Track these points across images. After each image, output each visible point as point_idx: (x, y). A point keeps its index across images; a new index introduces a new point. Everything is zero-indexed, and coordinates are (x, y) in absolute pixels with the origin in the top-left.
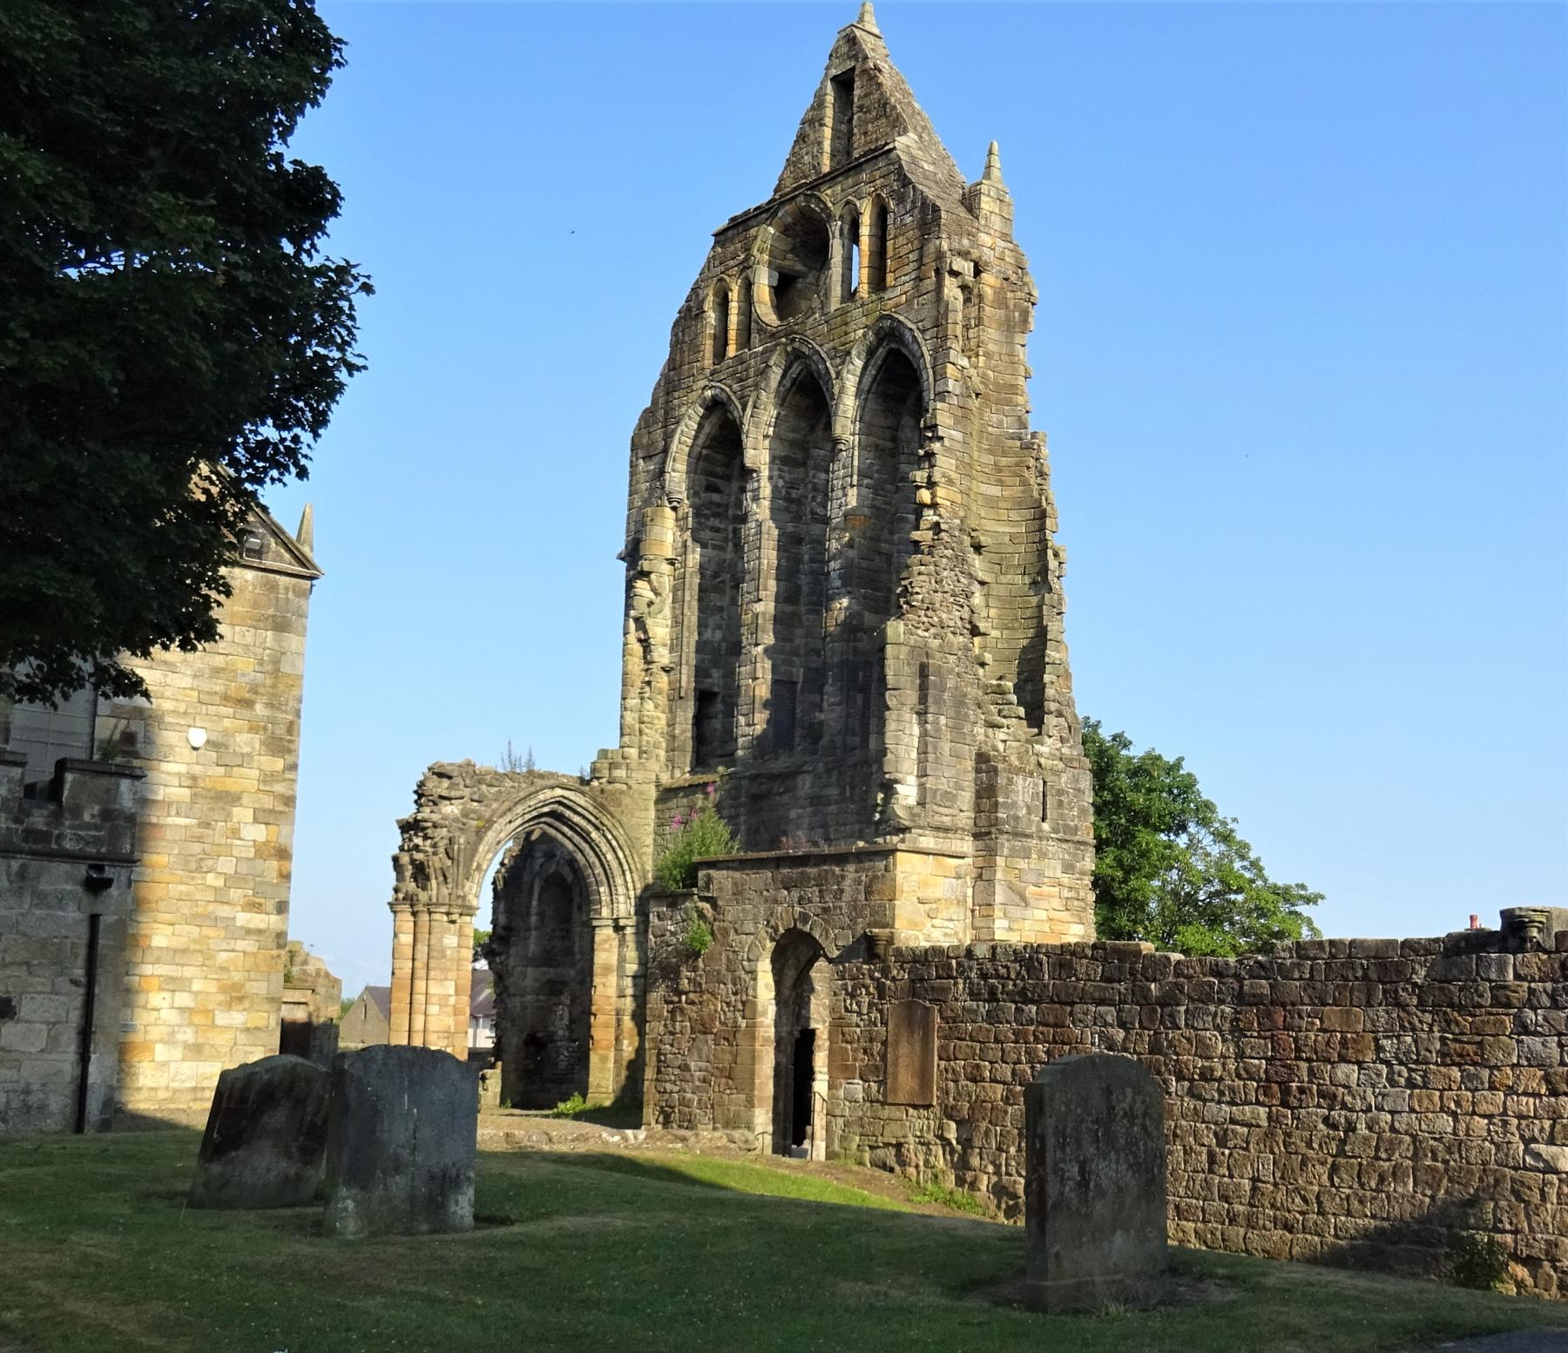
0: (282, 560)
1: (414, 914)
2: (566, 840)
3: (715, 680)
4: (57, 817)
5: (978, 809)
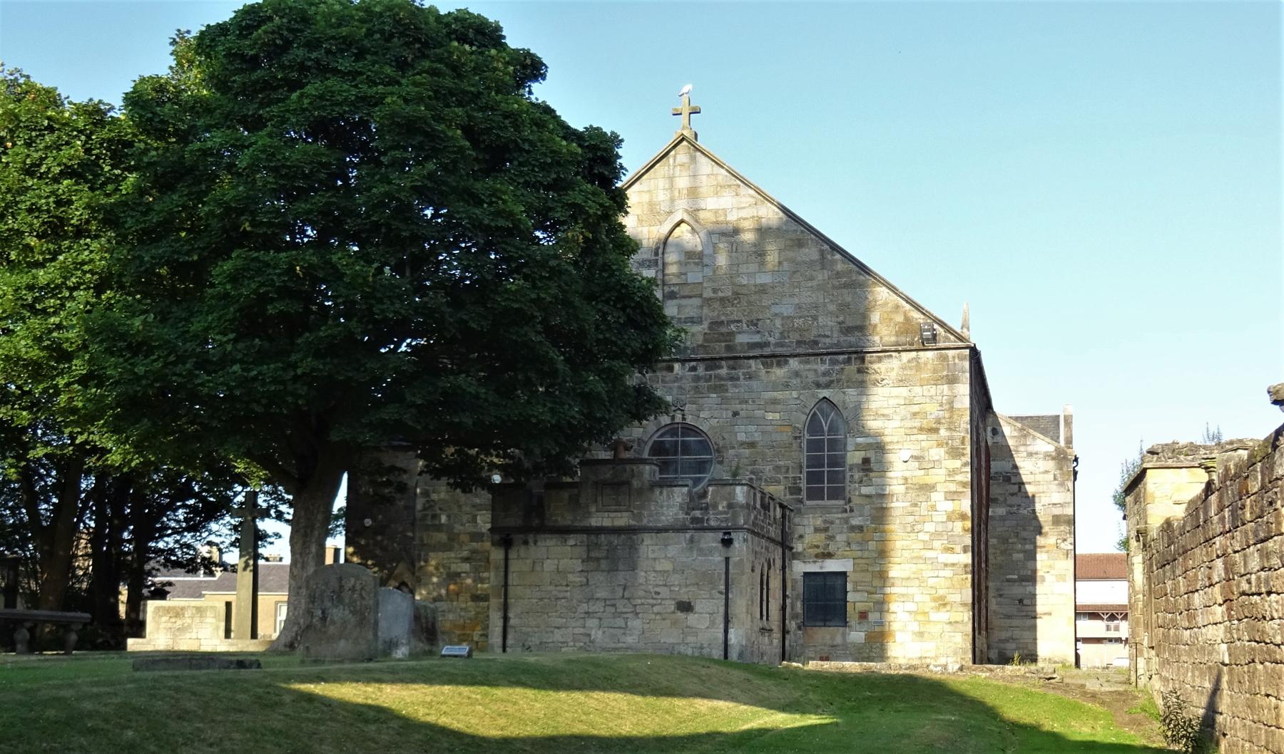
0: (949, 340)
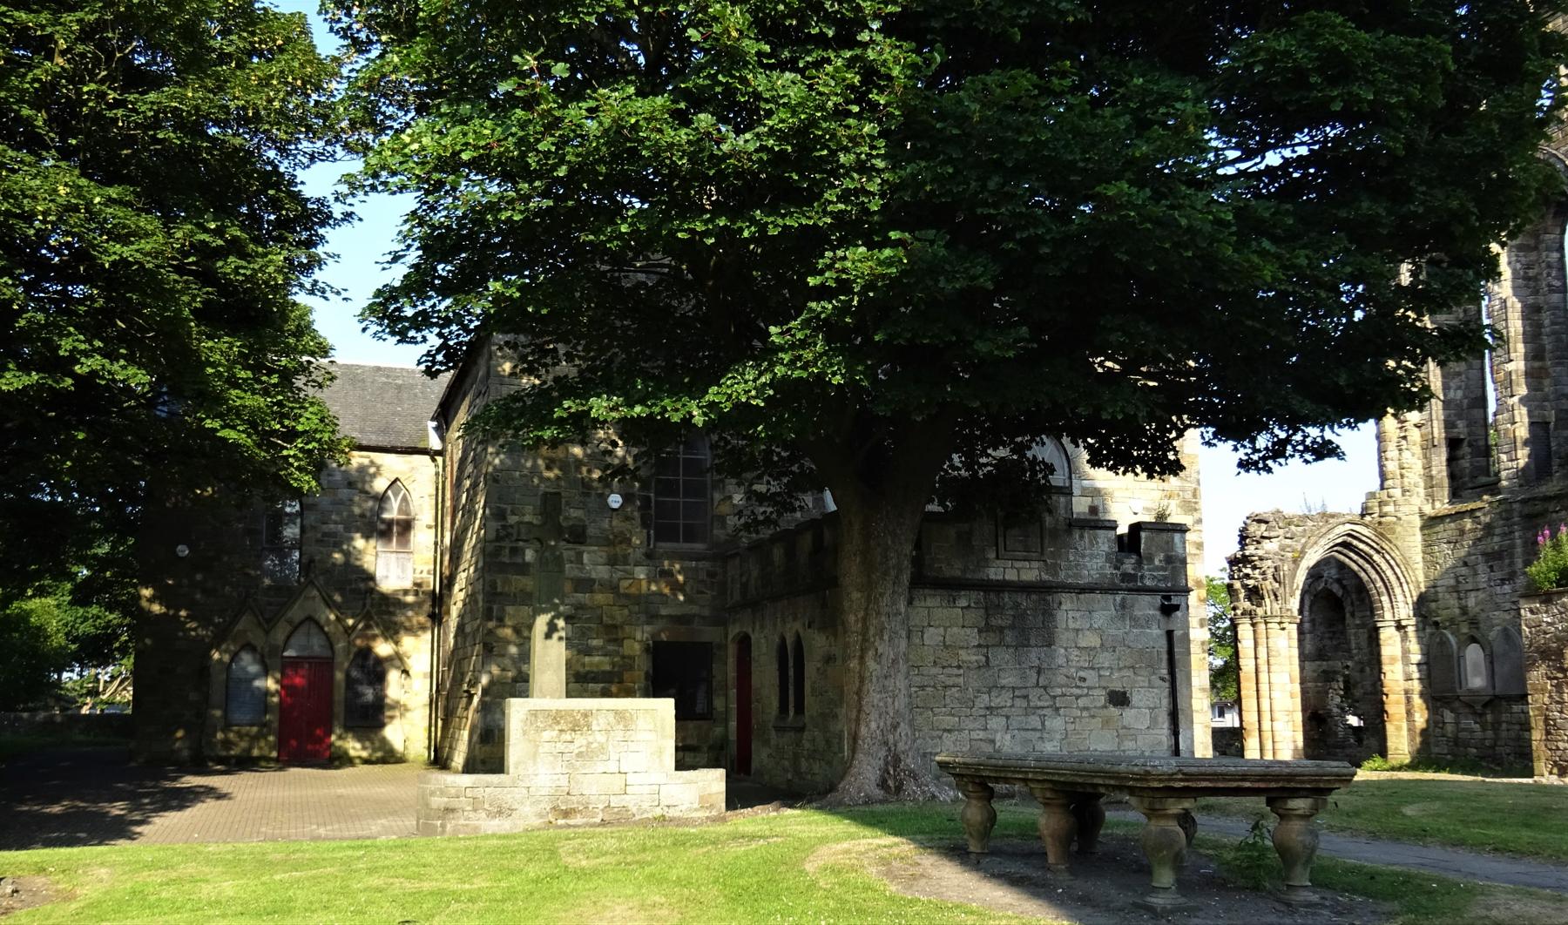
1: (1253, 625)
2: (1352, 562)
3: (1461, 428)
4: (1139, 563)
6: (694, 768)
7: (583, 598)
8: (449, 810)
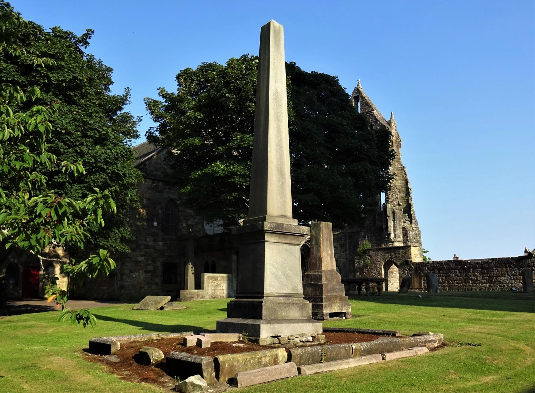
5: (403, 238)
6: (512, 258)
7: (147, 250)
8: (192, 297)
